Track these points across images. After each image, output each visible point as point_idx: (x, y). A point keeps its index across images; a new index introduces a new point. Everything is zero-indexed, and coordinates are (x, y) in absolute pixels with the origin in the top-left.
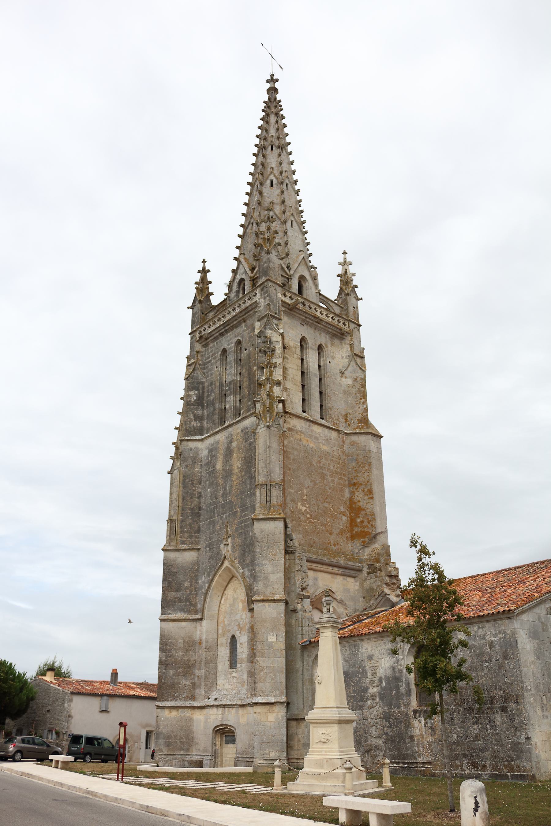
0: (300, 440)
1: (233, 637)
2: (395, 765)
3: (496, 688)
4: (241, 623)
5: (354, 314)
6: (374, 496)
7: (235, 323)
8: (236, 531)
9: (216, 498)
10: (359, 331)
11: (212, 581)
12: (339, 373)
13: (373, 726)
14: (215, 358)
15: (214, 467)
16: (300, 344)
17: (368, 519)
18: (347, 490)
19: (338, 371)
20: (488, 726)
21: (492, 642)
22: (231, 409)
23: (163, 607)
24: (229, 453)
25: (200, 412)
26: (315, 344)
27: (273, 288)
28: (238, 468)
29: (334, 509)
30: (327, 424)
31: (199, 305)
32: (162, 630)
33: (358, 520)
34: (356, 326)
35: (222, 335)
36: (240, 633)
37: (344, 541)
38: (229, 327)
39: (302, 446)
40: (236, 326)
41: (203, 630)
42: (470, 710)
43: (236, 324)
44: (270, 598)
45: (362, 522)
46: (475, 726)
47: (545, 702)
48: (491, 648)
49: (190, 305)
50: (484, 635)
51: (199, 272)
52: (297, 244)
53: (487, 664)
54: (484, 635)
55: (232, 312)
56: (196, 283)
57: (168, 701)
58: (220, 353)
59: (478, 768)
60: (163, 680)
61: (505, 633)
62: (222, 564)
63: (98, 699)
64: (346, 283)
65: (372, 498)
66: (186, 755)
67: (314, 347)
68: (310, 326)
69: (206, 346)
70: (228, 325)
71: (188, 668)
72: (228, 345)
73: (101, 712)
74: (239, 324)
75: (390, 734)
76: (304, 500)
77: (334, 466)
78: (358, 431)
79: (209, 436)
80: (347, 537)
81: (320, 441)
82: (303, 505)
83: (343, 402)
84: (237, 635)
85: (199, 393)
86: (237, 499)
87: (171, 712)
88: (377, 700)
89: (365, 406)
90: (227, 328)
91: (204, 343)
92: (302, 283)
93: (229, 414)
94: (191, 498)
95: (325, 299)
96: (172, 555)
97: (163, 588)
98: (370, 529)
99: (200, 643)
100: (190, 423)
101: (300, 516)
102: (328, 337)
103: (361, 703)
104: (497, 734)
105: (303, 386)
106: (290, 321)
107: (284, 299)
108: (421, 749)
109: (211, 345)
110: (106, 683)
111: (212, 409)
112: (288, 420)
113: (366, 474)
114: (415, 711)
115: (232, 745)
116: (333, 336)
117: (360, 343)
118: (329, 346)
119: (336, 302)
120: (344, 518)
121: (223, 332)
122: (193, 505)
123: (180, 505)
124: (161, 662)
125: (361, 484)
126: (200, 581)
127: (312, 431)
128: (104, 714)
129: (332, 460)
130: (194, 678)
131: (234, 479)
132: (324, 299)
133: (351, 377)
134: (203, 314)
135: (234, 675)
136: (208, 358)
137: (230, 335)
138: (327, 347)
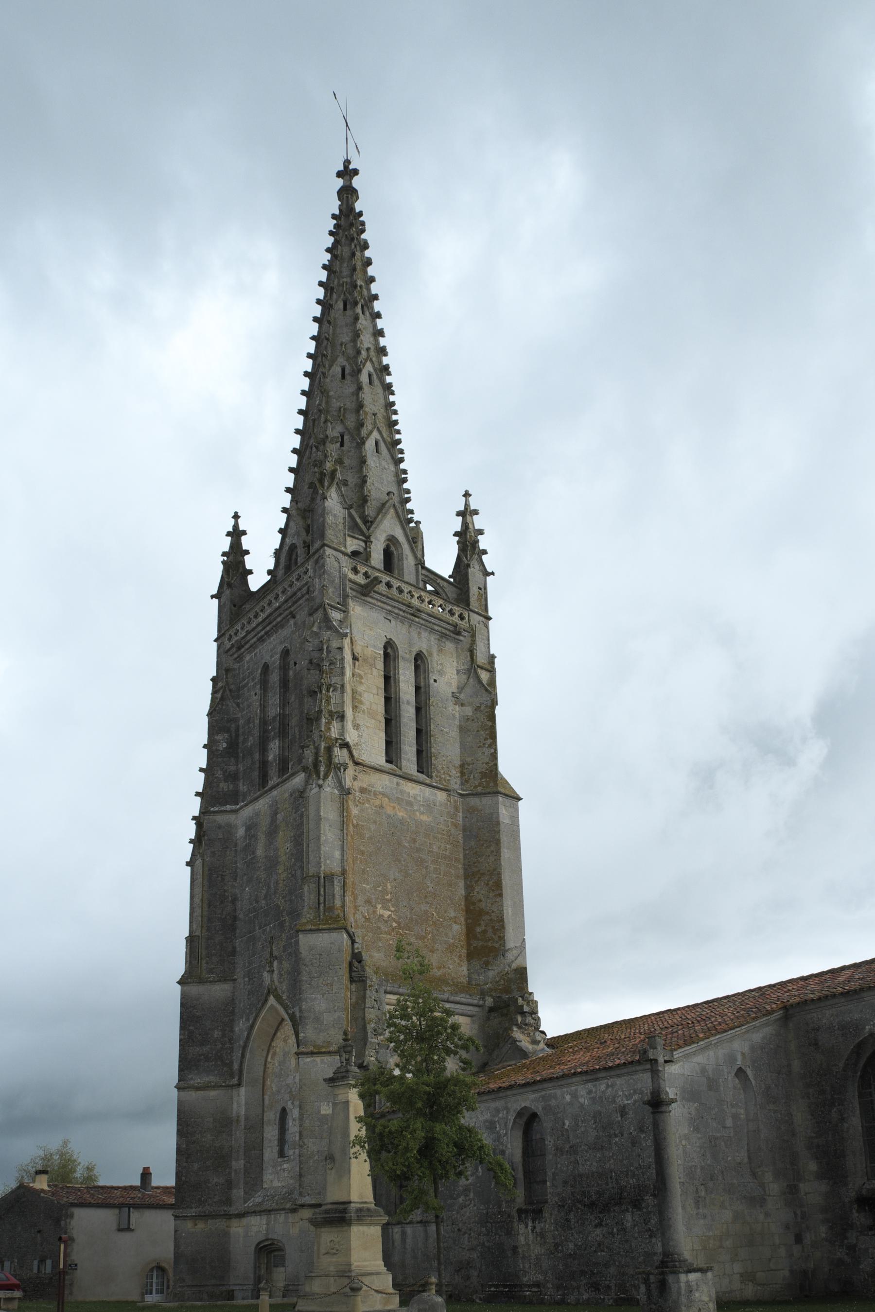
0: (381, 807)
1: (284, 1111)
2: (492, 1289)
3: (627, 1175)
4: (293, 1089)
5: (479, 600)
6: (504, 892)
7: (279, 619)
8: (284, 952)
9: (257, 902)
10: (487, 627)
11: (252, 1027)
12: (451, 698)
13: (465, 1233)
14: (253, 679)
15: (254, 853)
16: (382, 652)
17: (493, 927)
18: (461, 884)
19: (450, 695)
20: (615, 1230)
21: (624, 1106)
22: (275, 760)
23: (181, 1070)
24: (272, 832)
25: (232, 768)
26: (410, 652)
27: (332, 559)
28: (286, 854)
29: (438, 914)
30: (428, 781)
31: (228, 592)
32: (180, 1103)
33: (478, 930)
34: (482, 619)
35: (261, 640)
36: (293, 1103)
37: (455, 962)
38: (270, 626)
39: (384, 817)
40: (281, 626)
41: (241, 1101)
42: (592, 1205)
43: (282, 621)
44: (324, 1050)
45: (485, 932)
46: (598, 1231)
47: (703, 1194)
48: (622, 1116)
49: (215, 592)
50: (614, 1097)
51: (229, 534)
52: (385, 483)
53: (617, 1139)
54: (614, 1097)
55: (274, 601)
56: (224, 554)
57: (192, 1208)
58: (259, 671)
59: (599, 1290)
60: (183, 1178)
61: (642, 1093)
62: (266, 1000)
63: (116, 1211)
64: (468, 543)
65: (501, 895)
66: (220, 1285)
67: (407, 656)
68: (402, 622)
69: (240, 659)
70: (270, 624)
71: (222, 1160)
72: (272, 657)
73: (120, 1230)
74: (285, 620)
75: (487, 1244)
76: (387, 900)
77: (439, 848)
78: (479, 789)
79: (246, 805)
80: (460, 956)
81: (416, 808)
82: (385, 908)
83: (458, 745)
84: (289, 1105)
85: (231, 736)
86: (285, 901)
87: (196, 1225)
88: (472, 1195)
89: (493, 751)
90: (268, 628)
91: (236, 656)
92: (393, 548)
93: (273, 772)
94: (222, 902)
95: (432, 577)
96: (195, 990)
97: (180, 1040)
98: (497, 942)
99: (238, 1121)
100: (218, 786)
101: (380, 925)
102: (432, 639)
103: (449, 1202)
104: (627, 1241)
105: (388, 722)
106: (365, 614)
107: (351, 576)
108: (527, 1266)
109: (248, 658)
110: (132, 1188)
111: (250, 762)
112: (360, 776)
113: (492, 858)
114: (520, 1211)
115: (282, 1269)
116: (442, 637)
117: (489, 648)
118: (435, 655)
119: (452, 580)
120: (456, 927)
121: (261, 637)
122: (224, 913)
123: (205, 913)
124: (179, 1151)
125: (483, 874)
126: (237, 1029)
127: (402, 792)
128: (127, 1236)
129: (435, 837)
130: (230, 1173)
131: (280, 871)
132: (433, 577)
133: (470, 704)
134: (235, 606)
135: (285, 1166)
136: (244, 679)
137: (273, 640)
138: (431, 655)
